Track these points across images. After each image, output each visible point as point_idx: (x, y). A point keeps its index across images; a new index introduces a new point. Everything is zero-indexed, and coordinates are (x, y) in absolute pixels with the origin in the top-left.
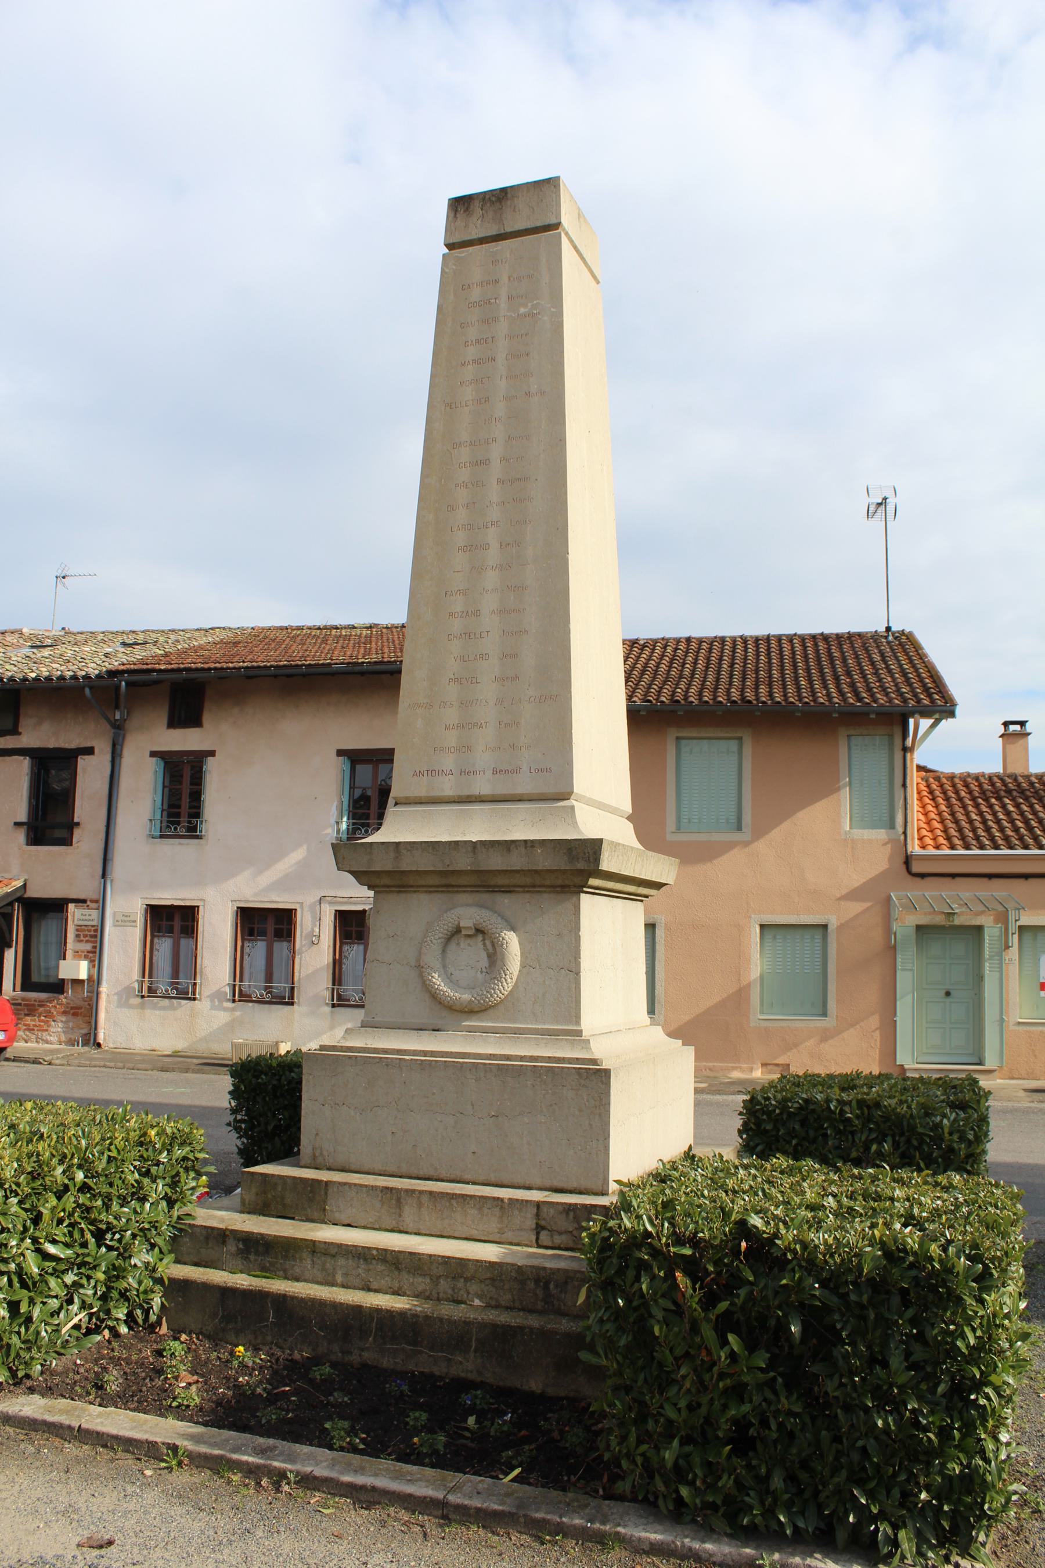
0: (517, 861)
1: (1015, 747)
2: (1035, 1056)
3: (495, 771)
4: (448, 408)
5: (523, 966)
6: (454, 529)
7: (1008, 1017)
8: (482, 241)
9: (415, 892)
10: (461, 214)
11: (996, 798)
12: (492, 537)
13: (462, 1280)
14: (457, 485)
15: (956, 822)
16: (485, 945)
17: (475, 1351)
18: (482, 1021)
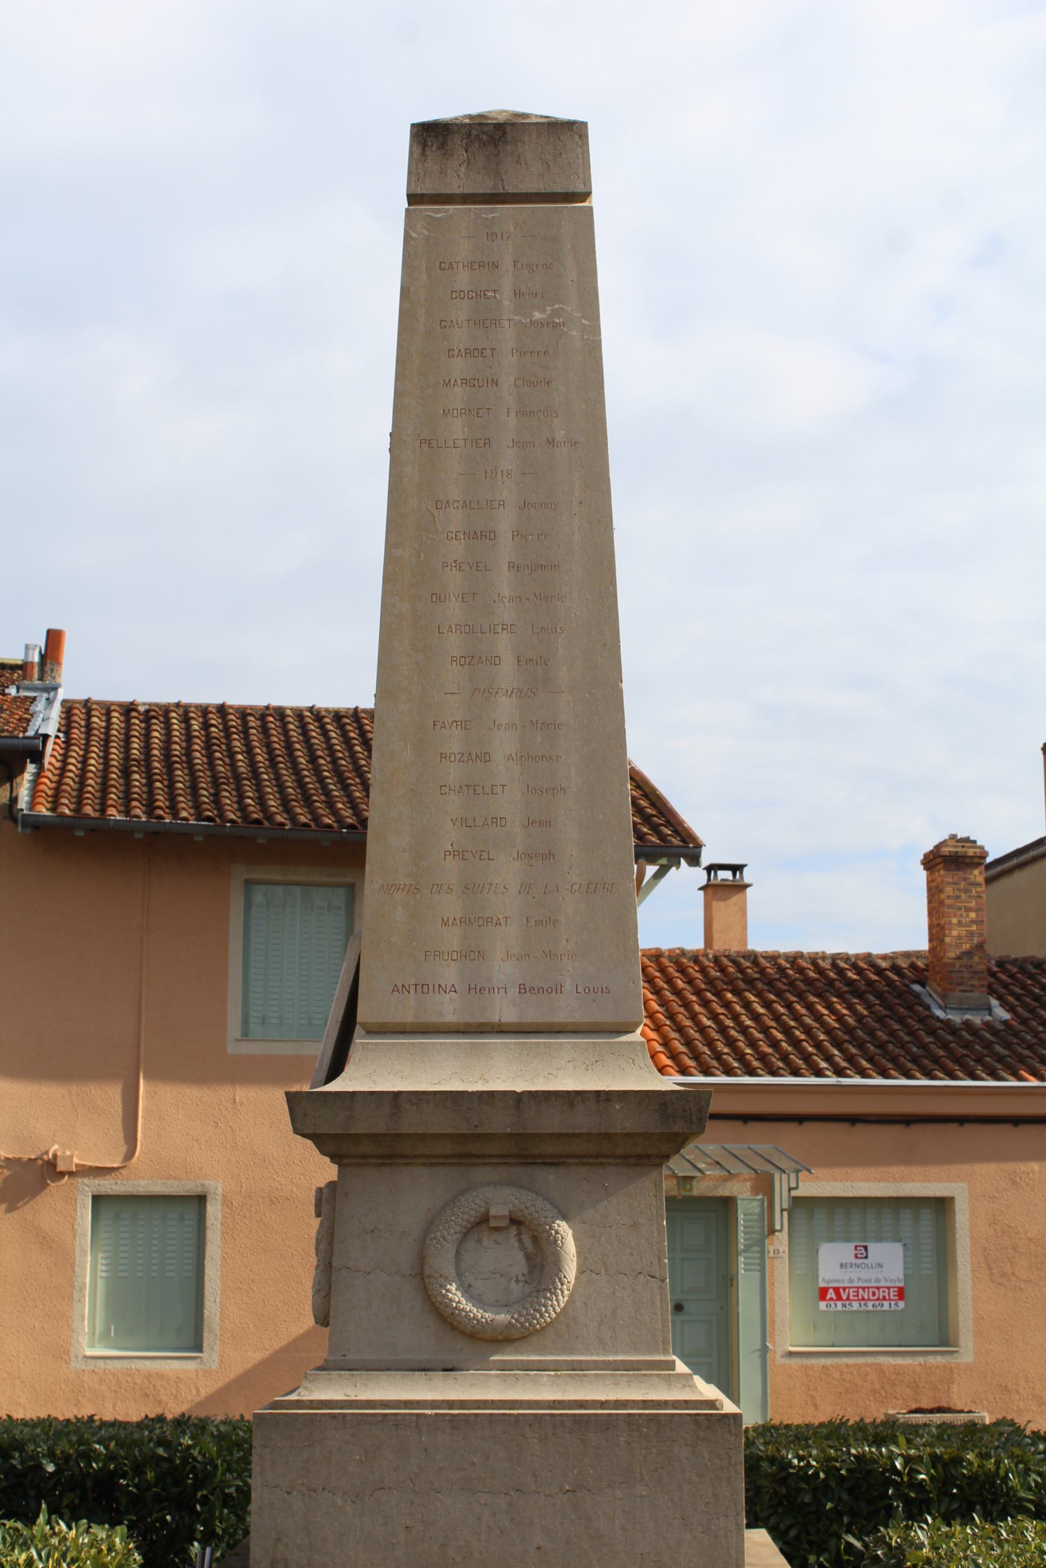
0: (583, 1121)
1: (723, 909)
2: (815, 1405)
3: (522, 989)
4: (425, 447)
5: (581, 1271)
7: (774, 1343)
9: (406, 1164)
10: (432, 152)
11: (732, 992)
12: (504, 645)
14: (445, 565)
15: (680, 1029)
18: (521, 1353)
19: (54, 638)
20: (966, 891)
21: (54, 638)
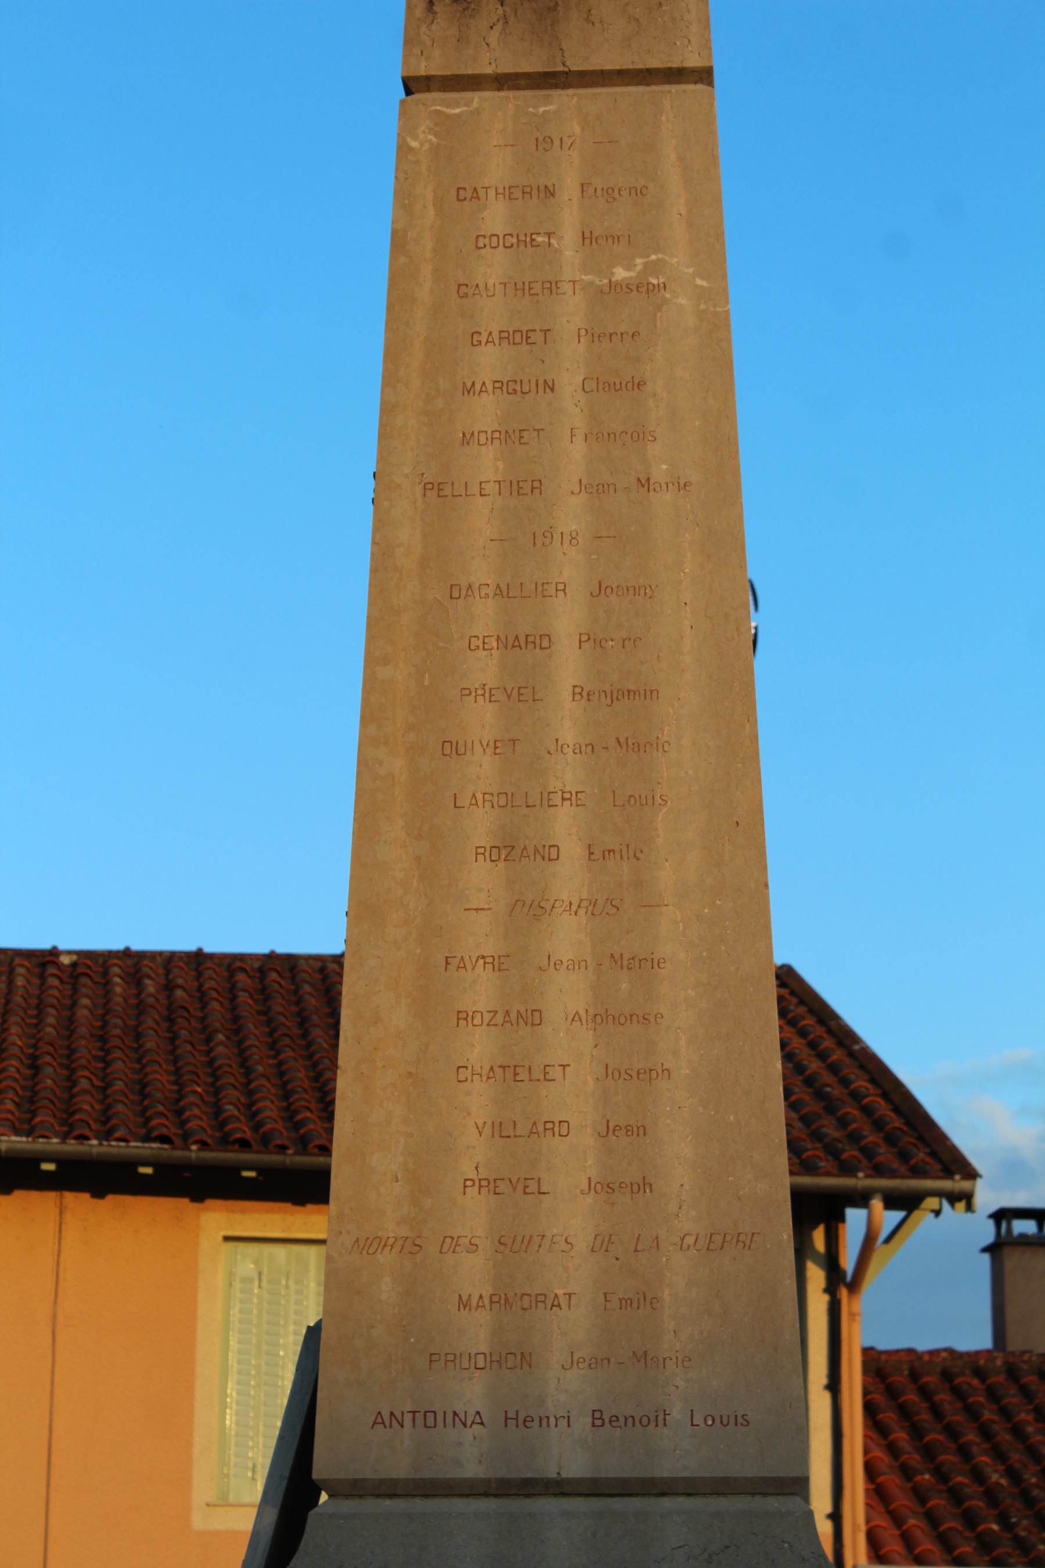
3: (598, 1418)
6: (465, 800)
8: (503, 82)
12: (566, 827)
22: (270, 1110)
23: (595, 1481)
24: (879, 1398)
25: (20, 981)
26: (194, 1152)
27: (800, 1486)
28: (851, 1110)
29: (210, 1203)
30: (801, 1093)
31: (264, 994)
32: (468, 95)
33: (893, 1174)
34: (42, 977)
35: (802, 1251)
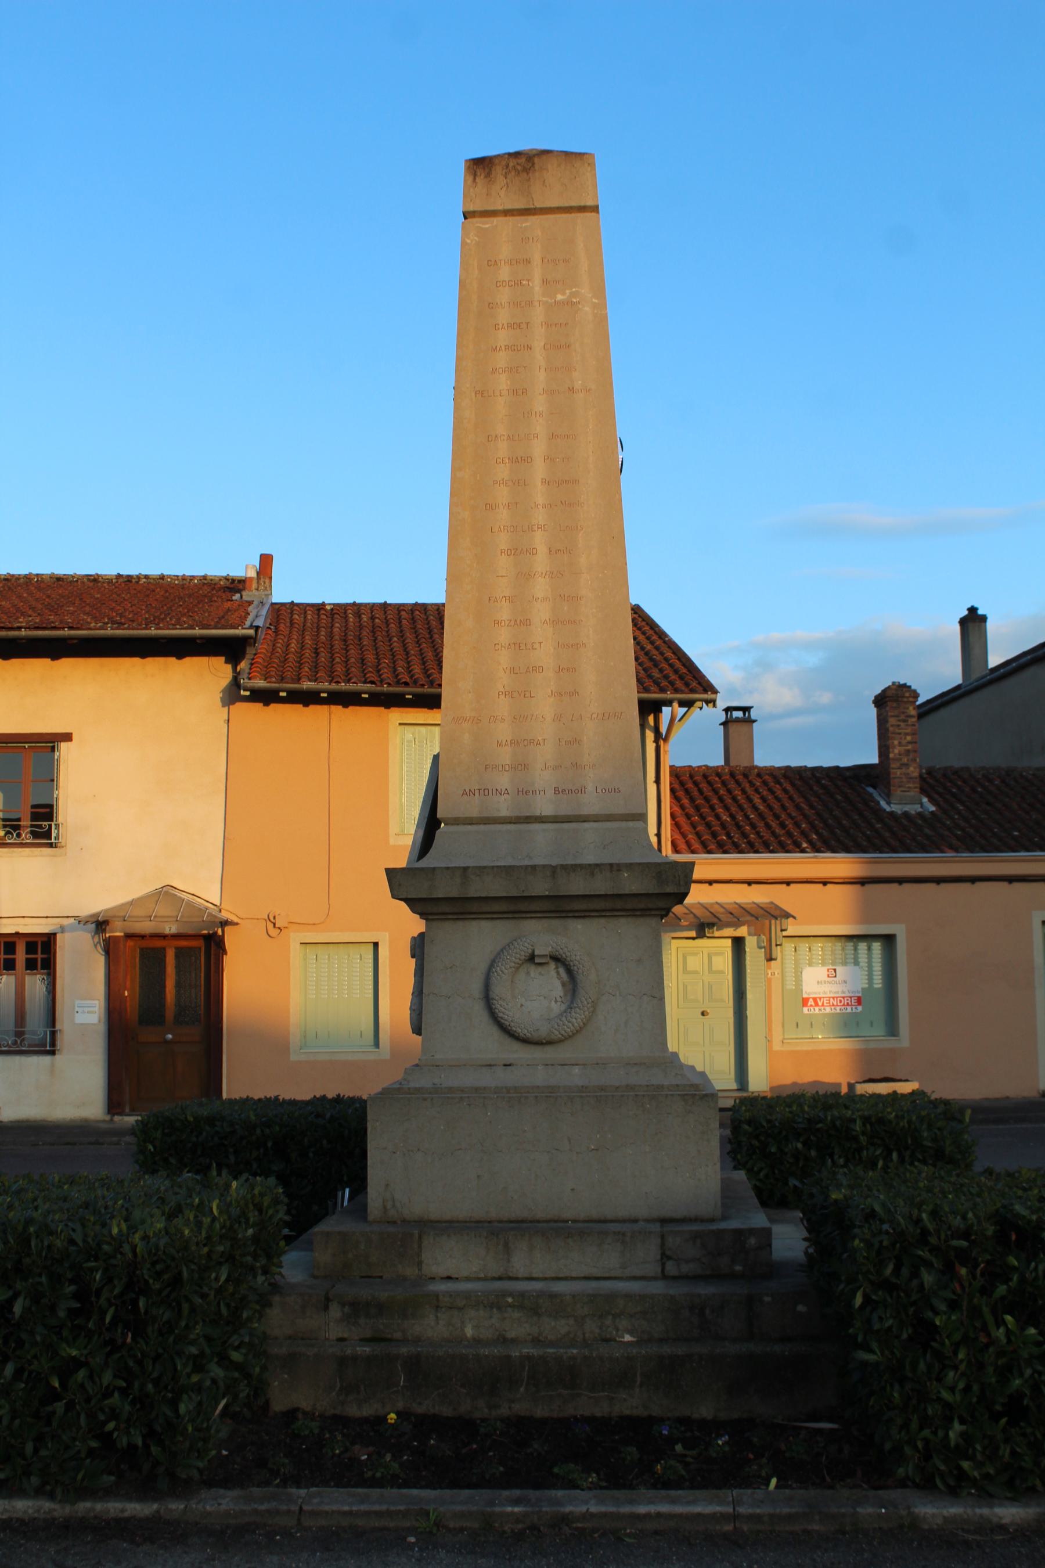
3: (557, 791)
6: (496, 529)
8: (507, 213)
12: (540, 541)
13: (610, 1317)
16: (558, 973)
17: (641, 1386)
19: (266, 561)
20: (904, 721)
21: (266, 561)
22: (417, 670)
23: (555, 817)
24: (677, 786)
25: (309, 617)
26: (385, 688)
27: (642, 817)
28: (664, 665)
29: (392, 709)
30: (643, 658)
31: (413, 620)
32: (492, 219)
33: (682, 692)
34: (319, 616)
35: (643, 726)
